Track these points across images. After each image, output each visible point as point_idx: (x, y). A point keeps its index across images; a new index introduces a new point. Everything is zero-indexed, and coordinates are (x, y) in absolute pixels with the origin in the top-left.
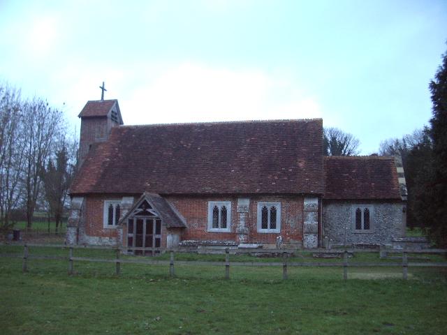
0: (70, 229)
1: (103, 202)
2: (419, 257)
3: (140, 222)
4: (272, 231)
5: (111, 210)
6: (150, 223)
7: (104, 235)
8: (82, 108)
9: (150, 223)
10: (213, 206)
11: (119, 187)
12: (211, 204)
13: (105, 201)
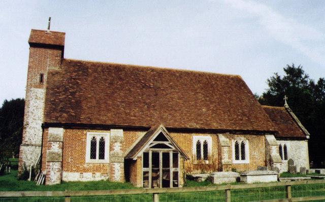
0: (51, 164)
1: (86, 135)
2: (283, 156)
3: (156, 155)
4: (101, 161)
5: (93, 144)
6: (166, 156)
7: (85, 170)
8: (250, 89)
9: (166, 156)
10: (92, 137)
11: (106, 118)
12: (90, 135)
13: (88, 133)
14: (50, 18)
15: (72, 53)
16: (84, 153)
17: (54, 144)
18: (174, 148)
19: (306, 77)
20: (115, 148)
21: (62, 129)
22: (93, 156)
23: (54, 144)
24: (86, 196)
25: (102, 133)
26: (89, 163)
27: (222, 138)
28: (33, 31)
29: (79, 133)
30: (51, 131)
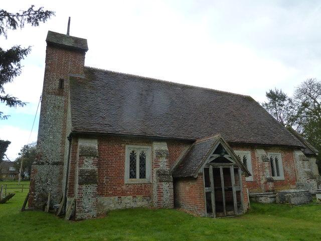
1: (124, 148)
6: (227, 171)
7: (124, 193)
10: (131, 151)
12: (128, 150)
13: (127, 146)
14: (70, 18)
15: (91, 60)
16: (123, 171)
17: (87, 160)
18: (235, 163)
19: (19, 154)
20: (160, 164)
21: (96, 141)
22: (132, 176)
23: (87, 160)
24: (65, 213)
25: (142, 147)
26: (129, 184)
27: (260, 153)
28: (49, 31)
29: (116, 146)
30: (82, 143)
